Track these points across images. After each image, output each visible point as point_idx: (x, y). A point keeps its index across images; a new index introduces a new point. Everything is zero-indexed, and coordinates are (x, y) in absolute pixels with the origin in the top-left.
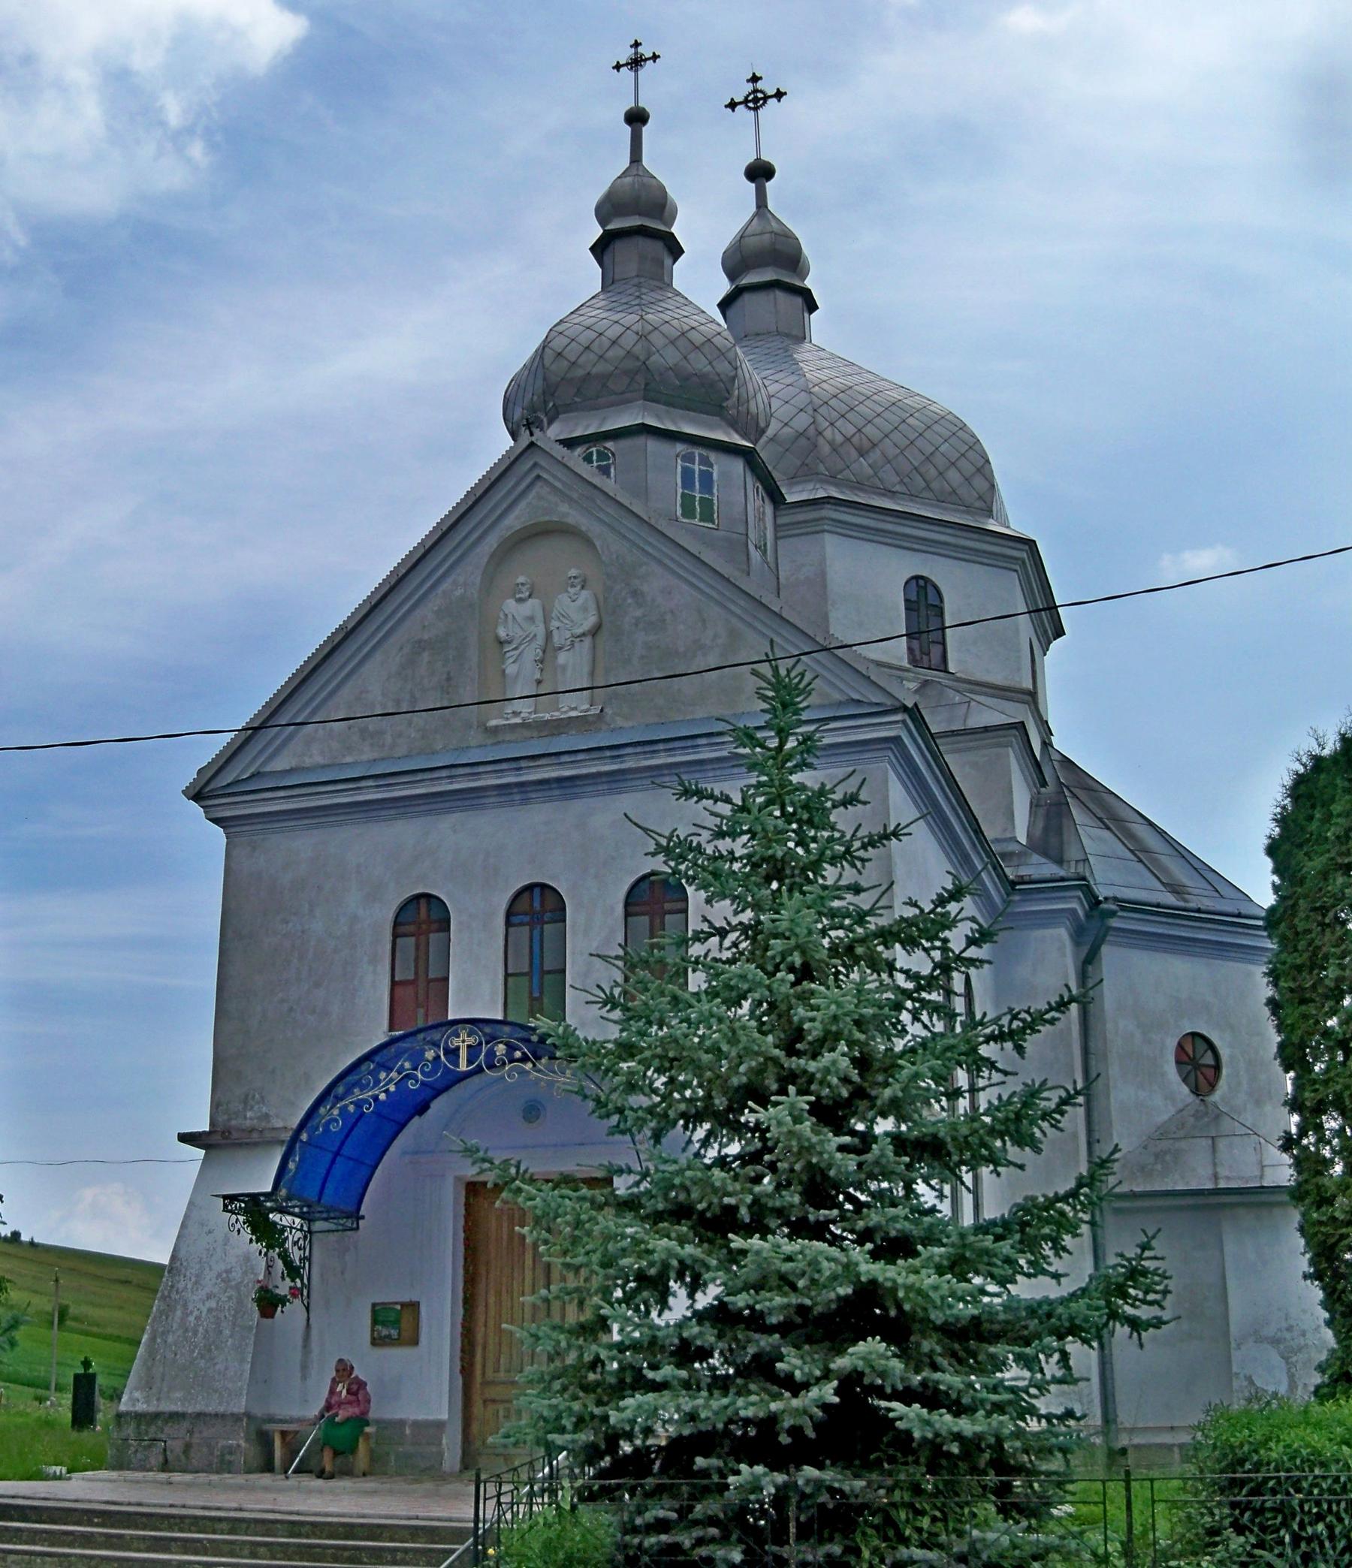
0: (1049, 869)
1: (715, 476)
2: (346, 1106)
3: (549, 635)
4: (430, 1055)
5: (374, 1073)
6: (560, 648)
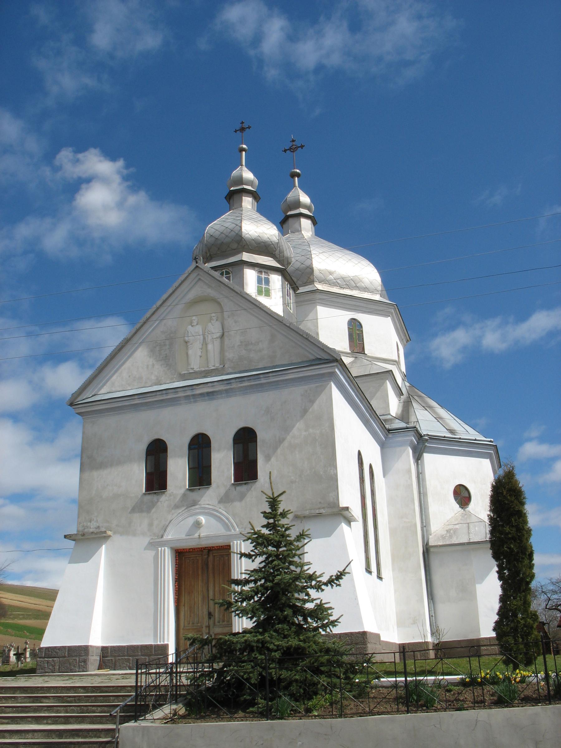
0: (403, 425)
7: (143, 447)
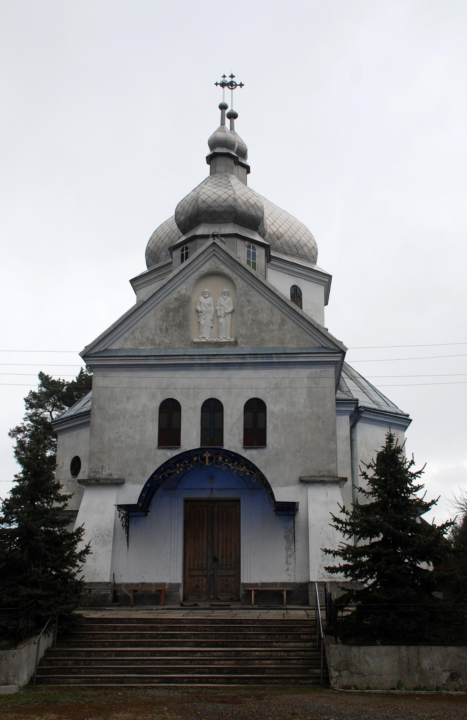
1: (257, 254)
2: (165, 475)
3: (216, 311)
4: (195, 459)
5: (175, 464)
6: (221, 317)
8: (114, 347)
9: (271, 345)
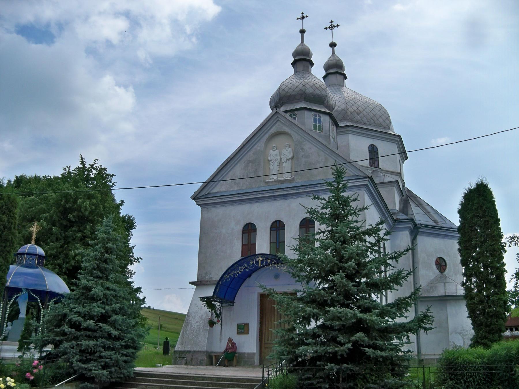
0: (403, 217)
3: (281, 159)
4: (251, 262)
5: (238, 267)
7: (240, 228)
8: (215, 191)
9: (318, 178)
